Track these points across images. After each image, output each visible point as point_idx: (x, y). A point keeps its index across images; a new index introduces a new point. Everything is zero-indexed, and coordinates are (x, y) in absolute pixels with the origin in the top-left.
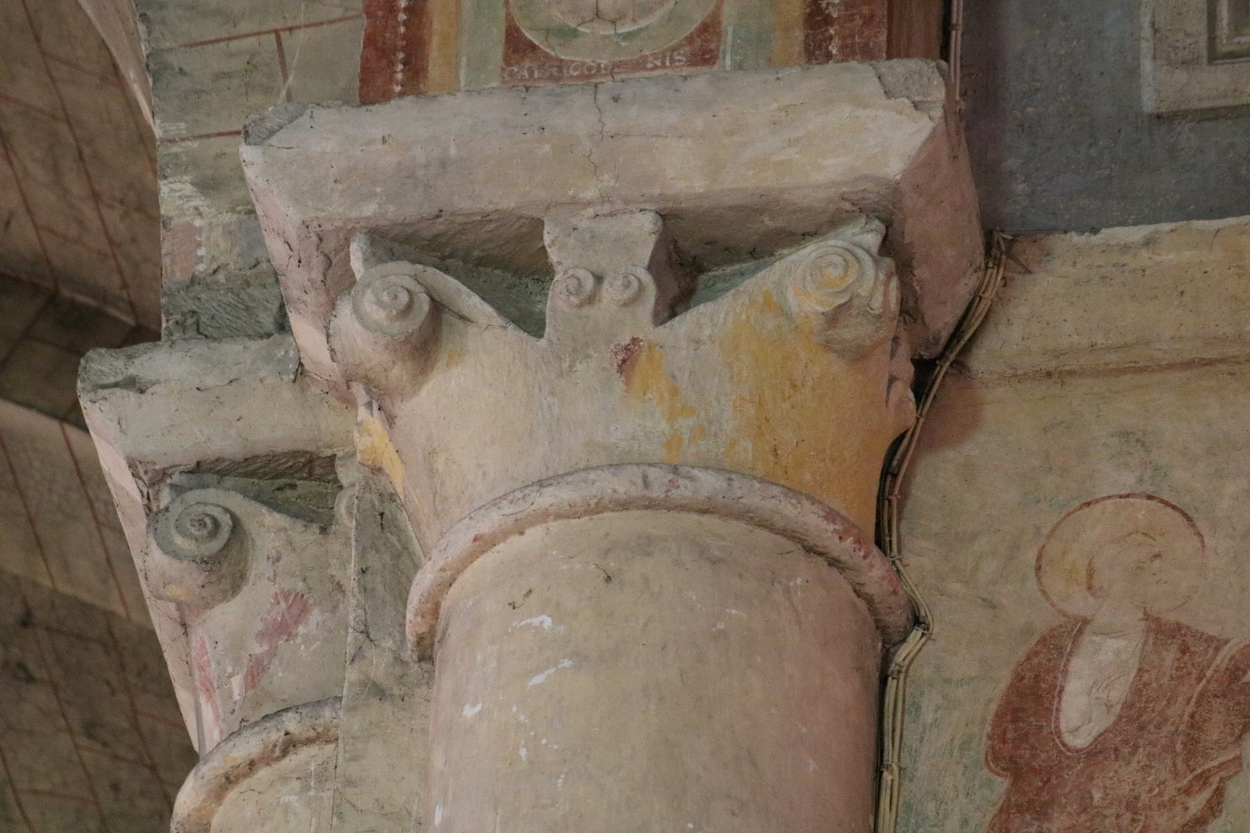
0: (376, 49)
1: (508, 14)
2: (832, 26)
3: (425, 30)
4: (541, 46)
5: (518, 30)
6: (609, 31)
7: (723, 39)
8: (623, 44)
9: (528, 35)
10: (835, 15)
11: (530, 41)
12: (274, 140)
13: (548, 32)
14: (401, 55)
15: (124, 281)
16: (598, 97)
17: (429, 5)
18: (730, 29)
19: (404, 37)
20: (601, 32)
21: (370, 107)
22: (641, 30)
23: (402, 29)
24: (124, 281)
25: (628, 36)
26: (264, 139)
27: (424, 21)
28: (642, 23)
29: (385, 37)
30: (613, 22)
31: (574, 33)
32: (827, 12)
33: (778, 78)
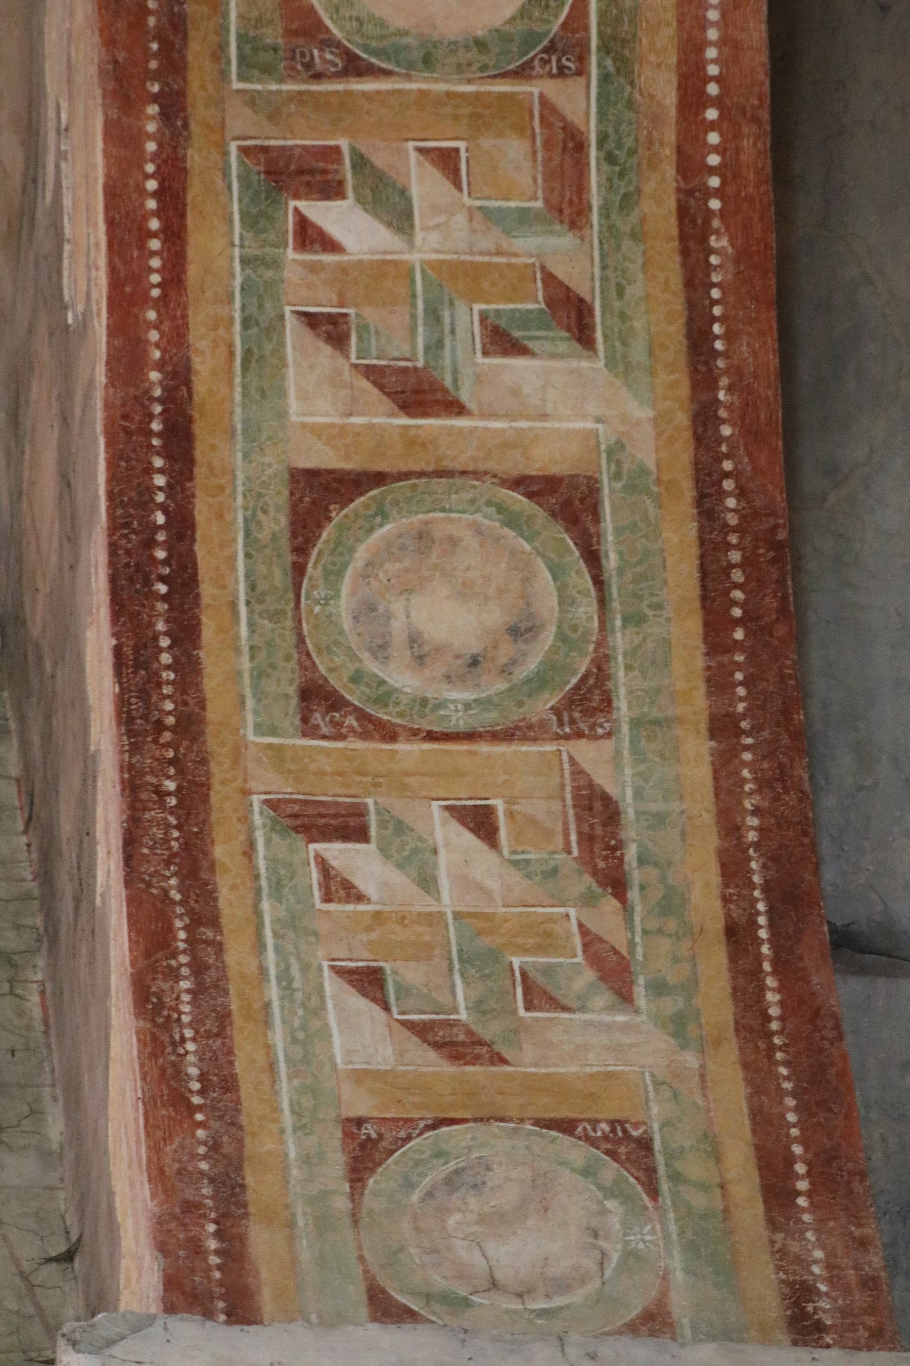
0: (183, 1294)
1: (366, 1272)
2: (827, 1334)
3: (250, 1279)
4: (422, 1312)
5: (383, 1291)
6: (516, 1305)
7: (678, 1331)
8: (539, 1322)
9: (399, 1297)
10: (829, 1323)
11: (405, 1306)
12: (116, 1350)
13: (428, 1297)
14: (221, 1305)
15: (686, 1181)
16: (567, 1350)
17: (251, 1250)
18: (686, 1322)
19: (221, 1283)
20: (505, 1306)
21: (246, 1328)
22: (560, 1309)
23: (217, 1275)
24: (686, 1181)
25: (543, 1313)
26: (101, 1349)
27: (248, 1267)
28: (559, 1301)
29: (194, 1281)
30: (520, 1295)
31: (466, 1303)
32: (816, 1317)
33: (814, 1359)
